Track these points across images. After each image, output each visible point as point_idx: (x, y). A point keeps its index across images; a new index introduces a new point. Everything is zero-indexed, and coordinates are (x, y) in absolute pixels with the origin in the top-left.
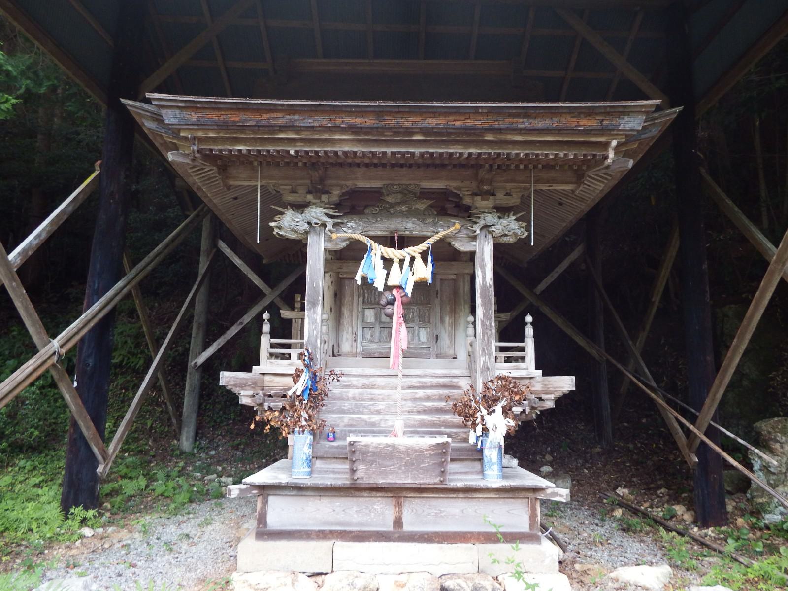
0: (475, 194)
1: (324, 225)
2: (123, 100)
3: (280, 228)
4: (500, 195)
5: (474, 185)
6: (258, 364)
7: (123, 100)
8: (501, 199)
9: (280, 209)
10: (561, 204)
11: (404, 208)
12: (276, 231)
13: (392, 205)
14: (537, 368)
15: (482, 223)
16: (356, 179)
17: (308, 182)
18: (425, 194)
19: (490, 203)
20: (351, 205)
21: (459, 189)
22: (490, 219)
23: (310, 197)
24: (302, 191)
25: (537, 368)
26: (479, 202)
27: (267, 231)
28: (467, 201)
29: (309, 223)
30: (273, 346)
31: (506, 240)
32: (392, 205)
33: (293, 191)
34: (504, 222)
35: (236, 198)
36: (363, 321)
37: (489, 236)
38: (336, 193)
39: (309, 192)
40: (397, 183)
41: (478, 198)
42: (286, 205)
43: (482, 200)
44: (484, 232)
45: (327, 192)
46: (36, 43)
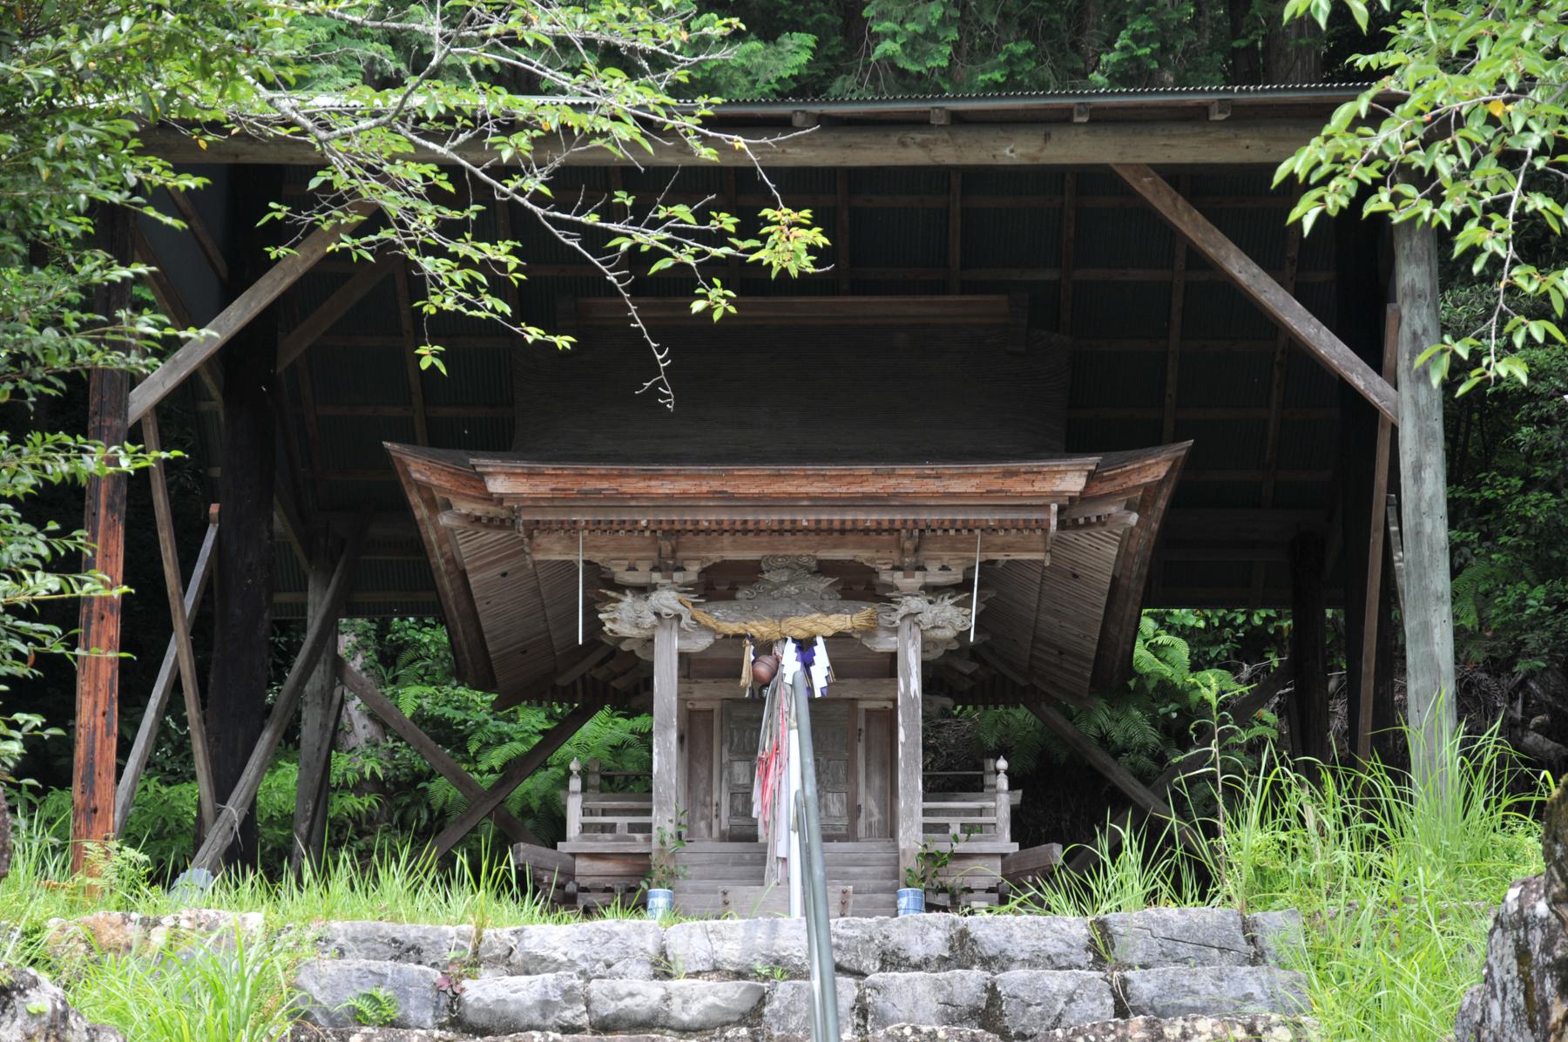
0: (895, 568)
1: (679, 617)
2: (387, 444)
3: (614, 621)
4: (933, 568)
5: (895, 555)
6: (564, 839)
7: (387, 444)
8: (935, 576)
9: (613, 594)
10: (1075, 576)
11: (793, 589)
12: (609, 625)
13: (777, 587)
14: (1013, 840)
15: (903, 610)
16: (722, 549)
17: (655, 554)
18: (824, 568)
19: (918, 579)
20: (718, 585)
21: (872, 560)
22: (915, 603)
23: (656, 577)
24: (644, 567)
25: (1013, 840)
26: (898, 578)
27: (594, 625)
28: (885, 577)
29: (657, 614)
30: (587, 812)
31: (939, 634)
32: (777, 587)
33: (632, 568)
34: (935, 609)
35: (504, 575)
36: (730, 781)
37: (916, 630)
38: (694, 569)
39: (655, 569)
40: (782, 553)
41: (900, 574)
42: (622, 588)
43: (905, 576)
44: (907, 622)
45: (681, 569)
46: (205, 338)
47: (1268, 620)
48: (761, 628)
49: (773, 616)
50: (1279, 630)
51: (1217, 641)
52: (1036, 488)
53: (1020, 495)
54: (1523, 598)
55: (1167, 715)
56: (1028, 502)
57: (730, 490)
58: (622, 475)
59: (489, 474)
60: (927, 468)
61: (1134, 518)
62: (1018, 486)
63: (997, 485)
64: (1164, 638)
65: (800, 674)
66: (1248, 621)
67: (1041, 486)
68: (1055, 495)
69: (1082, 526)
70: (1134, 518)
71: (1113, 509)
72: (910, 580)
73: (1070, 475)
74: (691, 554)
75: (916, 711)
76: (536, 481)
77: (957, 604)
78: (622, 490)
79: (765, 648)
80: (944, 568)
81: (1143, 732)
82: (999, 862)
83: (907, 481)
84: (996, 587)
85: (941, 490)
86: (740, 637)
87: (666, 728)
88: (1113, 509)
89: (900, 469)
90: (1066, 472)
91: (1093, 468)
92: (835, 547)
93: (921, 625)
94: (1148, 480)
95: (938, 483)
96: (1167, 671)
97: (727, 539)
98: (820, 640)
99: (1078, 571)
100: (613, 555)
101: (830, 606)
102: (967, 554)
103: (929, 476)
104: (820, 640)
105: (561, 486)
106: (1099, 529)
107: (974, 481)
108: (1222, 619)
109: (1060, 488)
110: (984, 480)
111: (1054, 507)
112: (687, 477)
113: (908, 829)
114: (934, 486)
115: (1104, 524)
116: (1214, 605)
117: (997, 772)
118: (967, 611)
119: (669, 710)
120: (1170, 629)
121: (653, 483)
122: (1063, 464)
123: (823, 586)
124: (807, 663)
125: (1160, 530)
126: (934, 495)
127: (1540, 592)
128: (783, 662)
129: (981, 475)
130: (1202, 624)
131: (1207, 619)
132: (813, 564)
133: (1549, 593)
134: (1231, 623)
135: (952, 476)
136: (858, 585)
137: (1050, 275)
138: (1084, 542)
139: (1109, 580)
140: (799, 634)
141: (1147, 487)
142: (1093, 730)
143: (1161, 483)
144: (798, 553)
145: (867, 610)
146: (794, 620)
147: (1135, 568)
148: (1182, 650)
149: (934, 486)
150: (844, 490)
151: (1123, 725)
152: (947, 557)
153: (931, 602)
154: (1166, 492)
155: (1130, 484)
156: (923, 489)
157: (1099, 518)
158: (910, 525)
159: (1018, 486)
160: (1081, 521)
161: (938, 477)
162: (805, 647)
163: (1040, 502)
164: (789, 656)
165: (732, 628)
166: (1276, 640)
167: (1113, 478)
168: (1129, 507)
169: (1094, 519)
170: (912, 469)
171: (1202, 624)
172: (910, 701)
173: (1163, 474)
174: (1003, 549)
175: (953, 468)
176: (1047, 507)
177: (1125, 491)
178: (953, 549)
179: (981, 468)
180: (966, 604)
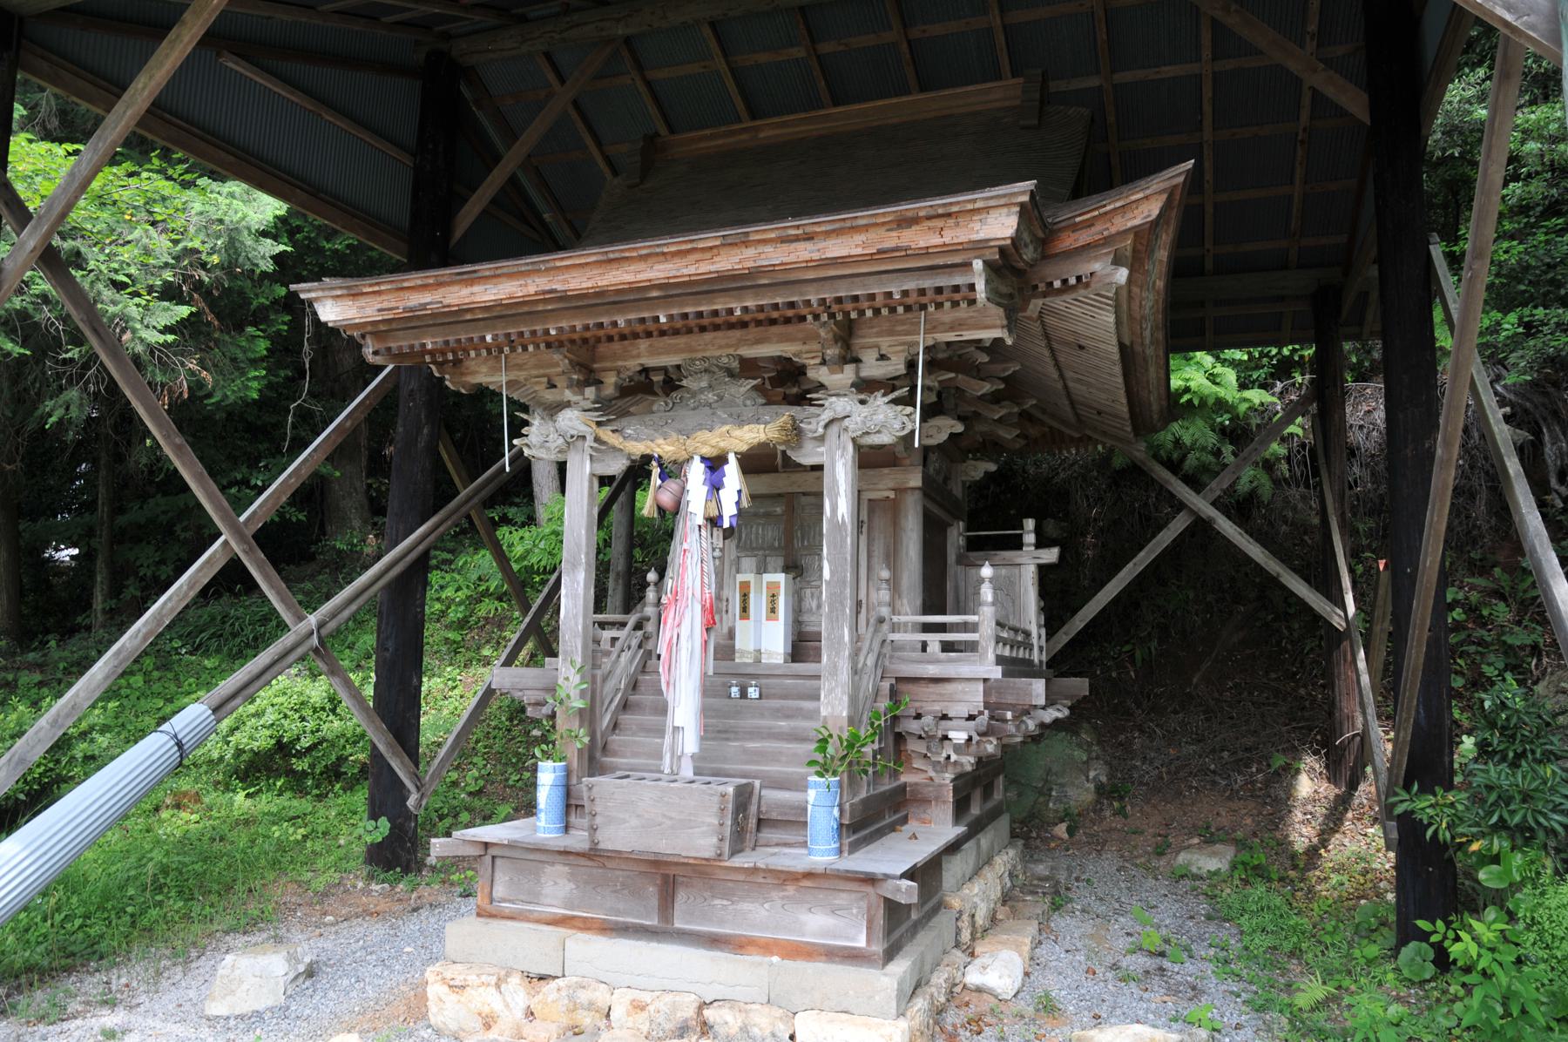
4: (869, 358)
8: (872, 368)
10: (1081, 347)
11: (711, 397)
15: (826, 416)
16: (638, 356)
18: (748, 367)
19: (848, 374)
32: (694, 394)
40: (699, 355)
43: (832, 372)
47: (1294, 351)
48: (665, 448)
49: (680, 432)
50: (1302, 357)
51: (1258, 367)
52: (947, 240)
53: (926, 252)
54: (1498, 323)
55: (1221, 423)
56: (940, 261)
57: (559, 287)
58: (440, 285)
59: (317, 299)
60: (790, 226)
61: (1122, 275)
62: (920, 238)
63: (891, 239)
64: (1219, 369)
65: (706, 498)
66: (1279, 353)
67: (956, 234)
68: (978, 246)
69: (1059, 292)
70: (1122, 275)
71: (1097, 266)
72: (839, 376)
73: (994, 214)
74: (608, 364)
75: (843, 540)
76: (362, 301)
77: (895, 402)
78: (446, 302)
79: (673, 470)
80: (882, 357)
81: (1204, 435)
82: (980, 687)
83: (769, 249)
84: (948, 379)
85: (816, 256)
86: (647, 459)
87: (574, 566)
88: (1097, 266)
89: (756, 231)
90: (987, 209)
91: (1026, 198)
92: (759, 342)
93: (850, 427)
94: (1137, 222)
95: (809, 245)
96: (1221, 392)
97: (643, 344)
98: (732, 458)
99: (1083, 342)
100: (535, 372)
101: (748, 412)
102: (909, 338)
103: (797, 239)
104: (732, 458)
105: (385, 305)
106: (1082, 292)
107: (859, 238)
108: (1261, 353)
109: (982, 235)
110: (872, 235)
111: (978, 265)
112: (511, 276)
113: (831, 691)
114: (804, 252)
115: (1087, 285)
116: (1255, 345)
117: (982, 581)
118: (909, 409)
119: (578, 545)
120: (1224, 362)
121: (476, 289)
122: (980, 197)
123: (743, 390)
124: (716, 487)
125: (1166, 286)
126: (810, 265)
127: (1512, 318)
128: (689, 487)
129: (866, 228)
130: (1246, 357)
131: (1249, 353)
132: (735, 364)
133: (1520, 318)
134: (1267, 355)
135: (828, 234)
136: (788, 385)
137: (1094, 82)
138: (1076, 310)
139: (1116, 350)
140: (708, 451)
141: (1137, 232)
142: (1170, 437)
143: (1155, 225)
144: (717, 353)
145: (786, 414)
146: (703, 435)
147: (1147, 333)
148: (1230, 376)
149: (804, 252)
150: (692, 270)
151: (1191, 431)
152: (885, 343)
153: (862, 402)
154: (1166, 238)
155: (1113, 230)
156: (792, 258)
157: (1079, 278)
158: (879, 300)
159: (920, 238)
160: (1057, 284)
161: (809, 238)
162: (715, 464)
163: (957, 259)
164: (696, 473)
165: (638, 448)
166: (1300, 364)
167: (1089, 224)
168: (1117, 262)
169: (1073, 281)
170: (770, 230)
171: (1246, 357)
172: (838, 527)
173: (1156, 212)
174: (952, 329)
175: (824, 222)
176: (967, 265)
177: (1107, 241)
178: (891, 333)
179: (863, 216)
180: (909, 401)
